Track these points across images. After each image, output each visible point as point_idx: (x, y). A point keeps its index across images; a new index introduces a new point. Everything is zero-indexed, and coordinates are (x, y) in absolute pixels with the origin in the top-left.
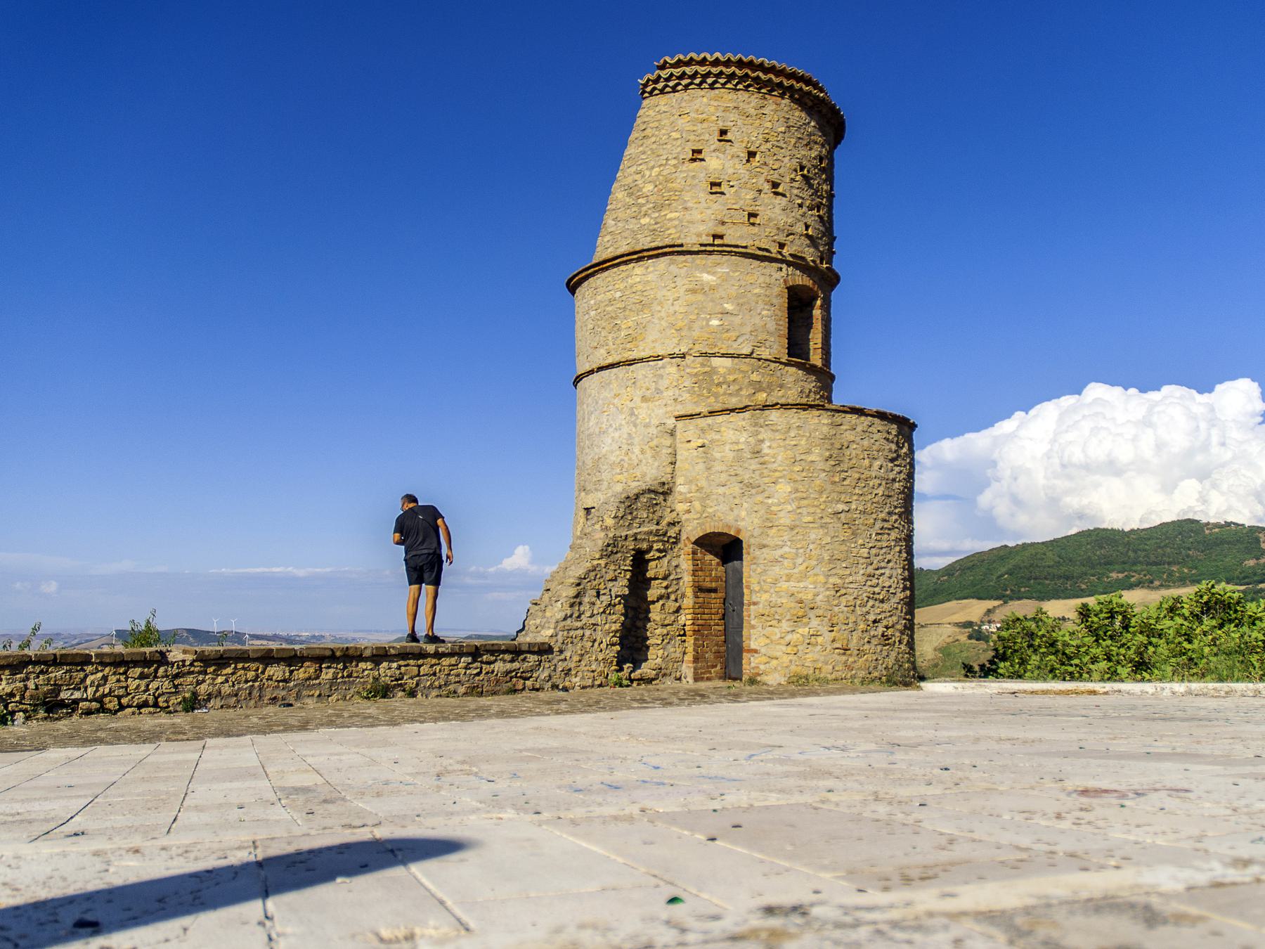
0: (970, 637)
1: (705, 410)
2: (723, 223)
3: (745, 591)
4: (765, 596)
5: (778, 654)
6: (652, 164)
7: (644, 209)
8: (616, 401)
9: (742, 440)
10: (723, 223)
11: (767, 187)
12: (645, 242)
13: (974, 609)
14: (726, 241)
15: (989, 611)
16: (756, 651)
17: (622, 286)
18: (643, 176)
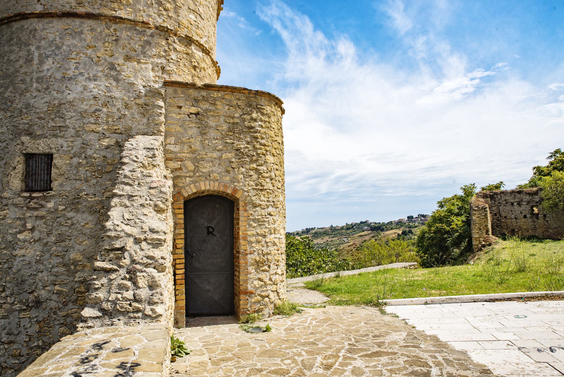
8: (89, 52)
9: (237, 115)
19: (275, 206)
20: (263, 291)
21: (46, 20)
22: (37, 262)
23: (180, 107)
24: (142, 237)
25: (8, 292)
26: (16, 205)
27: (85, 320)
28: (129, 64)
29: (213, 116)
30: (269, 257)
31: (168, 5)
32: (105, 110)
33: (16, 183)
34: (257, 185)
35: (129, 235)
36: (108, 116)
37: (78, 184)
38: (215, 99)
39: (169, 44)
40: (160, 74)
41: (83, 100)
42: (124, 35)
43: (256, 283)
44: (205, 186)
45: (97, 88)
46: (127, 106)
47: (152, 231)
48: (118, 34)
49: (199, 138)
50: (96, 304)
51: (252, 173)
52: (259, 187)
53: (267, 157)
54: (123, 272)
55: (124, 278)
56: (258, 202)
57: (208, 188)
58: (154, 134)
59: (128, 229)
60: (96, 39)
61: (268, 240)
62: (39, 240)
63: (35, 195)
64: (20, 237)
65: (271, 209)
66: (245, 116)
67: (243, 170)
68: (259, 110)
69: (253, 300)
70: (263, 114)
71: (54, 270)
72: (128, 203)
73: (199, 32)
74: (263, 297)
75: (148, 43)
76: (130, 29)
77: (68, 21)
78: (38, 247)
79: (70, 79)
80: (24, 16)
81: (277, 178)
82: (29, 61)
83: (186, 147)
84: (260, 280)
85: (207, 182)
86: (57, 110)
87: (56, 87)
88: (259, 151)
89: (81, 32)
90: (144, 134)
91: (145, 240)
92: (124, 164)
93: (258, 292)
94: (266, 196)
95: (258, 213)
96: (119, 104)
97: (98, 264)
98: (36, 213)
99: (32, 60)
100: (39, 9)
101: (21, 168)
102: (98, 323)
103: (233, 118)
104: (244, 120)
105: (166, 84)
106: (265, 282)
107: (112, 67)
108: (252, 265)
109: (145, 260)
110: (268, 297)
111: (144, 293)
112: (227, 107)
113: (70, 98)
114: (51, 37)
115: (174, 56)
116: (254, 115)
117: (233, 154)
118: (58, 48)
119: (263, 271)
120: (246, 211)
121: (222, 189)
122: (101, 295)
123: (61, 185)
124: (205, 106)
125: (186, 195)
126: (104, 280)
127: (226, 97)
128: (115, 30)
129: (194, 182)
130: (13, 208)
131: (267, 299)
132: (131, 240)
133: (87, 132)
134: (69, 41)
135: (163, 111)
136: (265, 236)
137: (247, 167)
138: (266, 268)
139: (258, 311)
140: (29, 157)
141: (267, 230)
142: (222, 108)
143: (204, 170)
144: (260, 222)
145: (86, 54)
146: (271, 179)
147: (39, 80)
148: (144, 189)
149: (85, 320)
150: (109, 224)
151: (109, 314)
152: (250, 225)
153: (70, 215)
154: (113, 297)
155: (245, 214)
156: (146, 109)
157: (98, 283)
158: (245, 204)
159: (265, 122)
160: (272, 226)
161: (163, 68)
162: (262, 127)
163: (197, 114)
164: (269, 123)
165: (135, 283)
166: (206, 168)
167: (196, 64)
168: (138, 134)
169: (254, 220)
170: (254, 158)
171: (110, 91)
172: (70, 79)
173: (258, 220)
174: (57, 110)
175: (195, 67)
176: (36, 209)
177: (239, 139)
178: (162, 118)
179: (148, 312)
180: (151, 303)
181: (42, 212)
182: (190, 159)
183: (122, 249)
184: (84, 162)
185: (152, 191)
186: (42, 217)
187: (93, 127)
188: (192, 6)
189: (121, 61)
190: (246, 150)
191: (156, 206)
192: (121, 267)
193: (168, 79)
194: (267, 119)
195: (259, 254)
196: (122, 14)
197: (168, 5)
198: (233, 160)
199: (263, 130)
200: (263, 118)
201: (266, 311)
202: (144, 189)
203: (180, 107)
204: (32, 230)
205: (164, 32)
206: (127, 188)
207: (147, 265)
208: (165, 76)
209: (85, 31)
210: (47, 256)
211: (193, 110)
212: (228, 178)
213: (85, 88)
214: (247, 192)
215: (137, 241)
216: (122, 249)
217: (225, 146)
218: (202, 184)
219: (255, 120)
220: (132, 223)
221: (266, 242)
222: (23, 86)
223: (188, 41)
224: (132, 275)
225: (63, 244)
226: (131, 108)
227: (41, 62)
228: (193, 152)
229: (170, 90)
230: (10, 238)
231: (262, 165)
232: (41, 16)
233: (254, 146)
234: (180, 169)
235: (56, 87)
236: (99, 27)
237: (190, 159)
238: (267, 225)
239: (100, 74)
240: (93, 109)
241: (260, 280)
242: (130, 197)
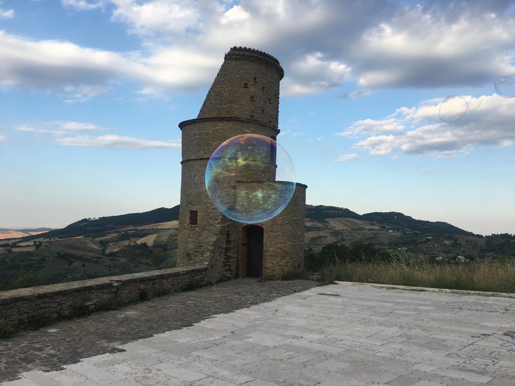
1: (249, 181)
2: (254, 112)
4: (272, 249)
5: (276, 269)
6: (228, 86)
7: (224, 102)
11: (267, 100)
12: (224, 114)
14: (255, 118)
16: (268, 268)
17: (213, 129)
18: (224, 89)
26: (187, 229)
33: (188, 221)
62: (194, 241)
64: (189, 240)
74: (273, 271)
118: (199, 171)
140: (191, 212)
176: (193, 230)
204: (192, 238)
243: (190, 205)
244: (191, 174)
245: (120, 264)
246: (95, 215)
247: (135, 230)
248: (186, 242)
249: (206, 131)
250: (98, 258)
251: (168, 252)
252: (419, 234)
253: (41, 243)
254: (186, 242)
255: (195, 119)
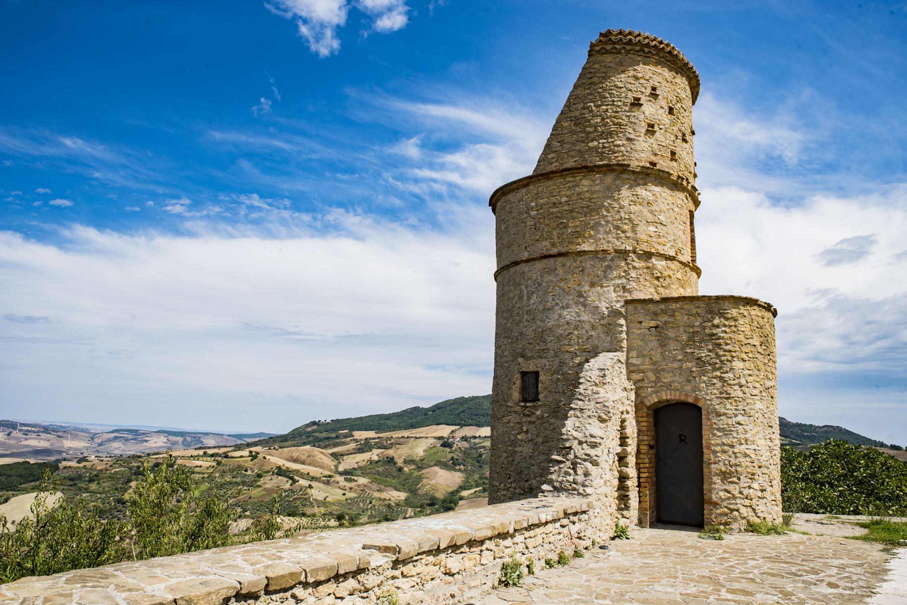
0: (442, 445)
3: (705, 450)
8: (562, 284)
9: (697, 324)
10: (656, 155)
13: (444, 431)
15: (453, 432)
19: (745, 413)
20: (731, 504)
21: (531, 263)
22: (530, 457)
23: (641, 322)
24: (584, 440)
25: (512, 479)
26: (516, 412)
27: (543, 492)
28: (594, 290)
29: (672, 327)
30: (739, 469)
31: (626, 227)
32: (576, 332)
33: (516, 395)
34: (721, 393)
35: (575, 438)
36: (578, 338)
37: (557, 396)
38: (674, 311)
39: (628, 264)
40: (621, 293)
41: (559, 326)
42: (588, 264)
43: (722, 494)
44: (666, 396)
45: (569, 315)
46: (593, 328)
47: (591, 436)
48: (583, 264)
49: (660, 350)
50: (550, 482)
51: (715, 381)
52: (724, 395)
53: (734, 363)
54: (568, 464)
55: (569, 468)
56: (723, 410)
57: (669, 397)
58: (616, 351)
59: (575, 434)
60: (566, 272)
61: (735, 451)
62: (532, 440)
63: (528, 404)
64: (519, 437)
65: (740, 418)
66: (705, 324)
67: (705, 378)
68: (722, 315)
69: (718, 511)
70: (727, 319)
71: (542, 465)
72: (579, 415)
73: (662, 240)
74: (732, 510)
75: (609, 267)
76: (593, 258)
77: (545, 261)
78: (530, 445)
79: (549, 310)
80: (516, 263)
81: (749, 385)
82: (521, 298)
83: (647, 360)
84: (726, 491)
85: (668, 392)
86: (541, 335)
87: (539, 317)
88: (723, 358)
89: (555, 269)
90: (609, 351)
91: (586, 442)
92: (580, 383)
93: (725, 503)
94: (734, 404)
95: (723, 422)
96: (587, 327)
97: (554, 457)
98: (529, 419)
99: (523, 297)
100: (526, 255)
101: (518, 382)
102: (550, 494)
103: (693, 327)
104: (704, 328)
105: (627, 302)
106: (733, 495)
107: (580, 295)
108: (716, 474)
109: (584, 457)
110: (737, 510)
111: (580, 478)
112: (686, 317)
113: (550, 325)
114: (534, 276)
115: (633, 274)
116: (716, 321)
117: (694, 364)
118: (540, 285)
119: (732, 482)
120: (709, 419)
121: (683, 398)
122: (554, 477)
123: (546, 397)
124: (665, 318)
125: (648, 404)
126: (556, 468)
127: (685, 307)
128: (581, 262)
129: (656, 392)
130: (514, 415)
131: (736, 513)
132: (577, 442)
133: (563, 352)
134: (547, 278)
135: (625, 328)
136: (732, 446)
137: (710, 375)
138: (735, 479)
139: (726, 524)
140: (524, 374)
141: (734, 440)
142: (682, 318)
143: (665, 381)
144: (726, 432)
145: (559, 287)
146: (741, 386)
147: (528, 312)
148: (593, 403)
149: (543, 492)
150: (564, 431)
151: (557, 490)
152: (714, 435)
153: (552, 421)
154: (560, 479)
155: (708, 423)
156: (610, 328)
157: (552, 470)
158: (708, 413)
159: (730, 326)
160: (742, 436)
161: (624, 288)
162: (726, 332)
163: (656, 327)
164: (735, 326)
165: (575, 472)
166: (667, 378)
167: (659, 275)
168: (603, 351)
169: (718, 429)
170: (717, 366)
171: (579, 316)
172: (549, 310)
173: (724, 430)
174: (541, 335)
175: (657, 278)
176: (528, 416)
177: (700, 348)
178: (624, 336)
179: (581, 491)
180: (584, 485)
181: (533, 419)
182: (652, 370)
183: (570, 448)
184: (562, 378)
185: (598, 405)
186: (533, 422)
187: (567, 348)
188: (650, 218)
189: (587, 288)
190: (708, 358)
191: (599, 417)
192: (568, 460)
193: (629, 298)
194: (733, 323)
195: (725, 464)
196: (586, 247)
197: (626, 227)
198: (694, 369)
199: (726, 336)
200: (726, 323)
201: (735, 526)
202: (593, 403)
203: (641, 322)
204: (527, 432)
205: (623, 254)
206: (580, 403)
207: (585, 460)
208: (626, 294)
209: (559, 268)
210: (537, 453)
211: (653, 323)
212: (688, 388)
213: (560, 315)
214: (710, 400)
215: (580, 443)
216: (570, 448)
217: (685, 356)
218: (663, 393)
219: (718, 326)
220: (579, 430)
221: (734, 453)
222: (518, 318)
223: (647, 255)
224: (574, 466)
225: (547, 444)
226: (597, 329)
227: (529, 298)
228: (654, 364)
229: (631, 307)
230: (513, 438)
231: (727, 372)
232: (528, 261)
233: (717, 354)
234: (643, 380)
235: (539, 317)
236: (568, 261)
237: (652, 370)
238: (735, 435)
239: (571, 302)
240: (567, 333)
241: (726, 491)
242: (581, 410)
243: (520, 360)
244: (521, 291)
245: (358, 486)
246: (327, 417)
247: (379, 438)
248: (514, 443)
249: (553, 200)
250: (330, 477)
251: (424, 471)
252: (799, 444)
253: (257, 453)
254: (514, 443)
255: (530, 177)
